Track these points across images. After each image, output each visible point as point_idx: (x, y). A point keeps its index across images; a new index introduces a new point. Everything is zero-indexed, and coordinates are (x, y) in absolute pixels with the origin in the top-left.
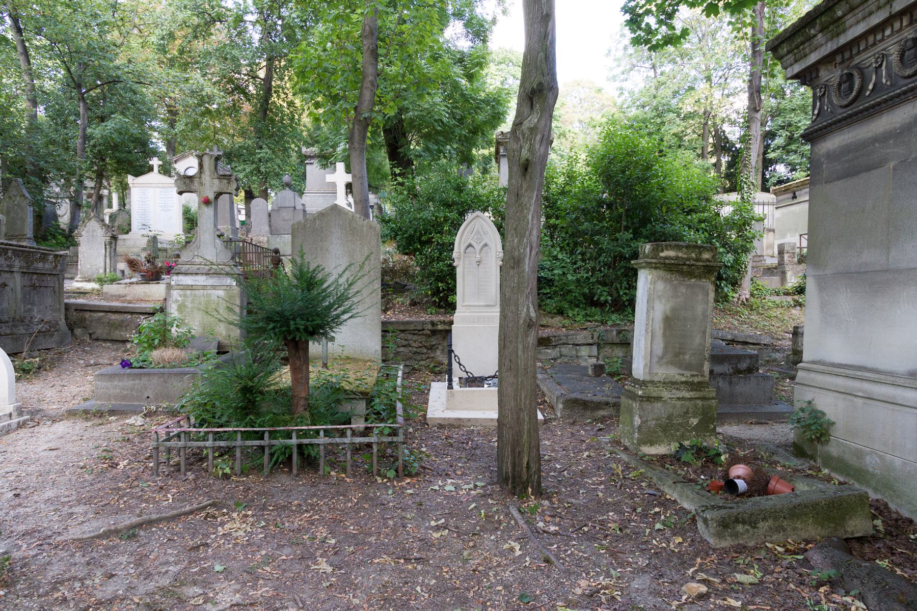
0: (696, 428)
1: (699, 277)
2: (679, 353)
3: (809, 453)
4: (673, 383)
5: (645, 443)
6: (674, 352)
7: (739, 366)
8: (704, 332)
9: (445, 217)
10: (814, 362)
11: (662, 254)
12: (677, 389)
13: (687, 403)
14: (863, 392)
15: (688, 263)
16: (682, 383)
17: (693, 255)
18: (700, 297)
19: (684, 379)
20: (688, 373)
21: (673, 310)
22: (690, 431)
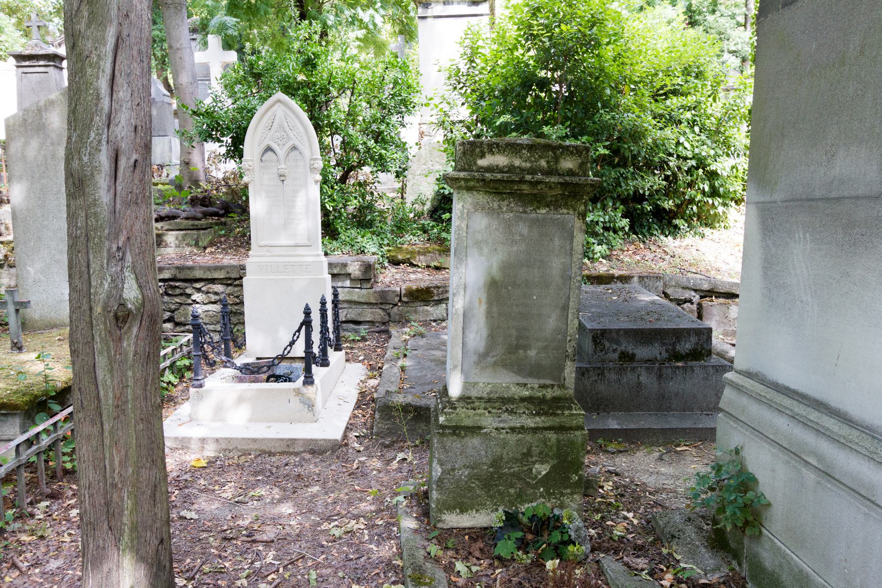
0: (545, 481)
1: (555, 204)
2: (518, 347)
3: (733, 545)
4: (504, 401)
5: (451, 508)
6: (508, 342)
7: (678, 347)
8: (565, 308)
10: (749, 375)
11: (482, 162)
12: (511, 412)
13: (529, 437)
14: (820, 458)
15: (528, 177)
16: (523, 399)
17: (543, 163)
18: (557, 242)
19: (526, 393)
20: (534, 383)
21: (506, 267)
22: (535, 487)
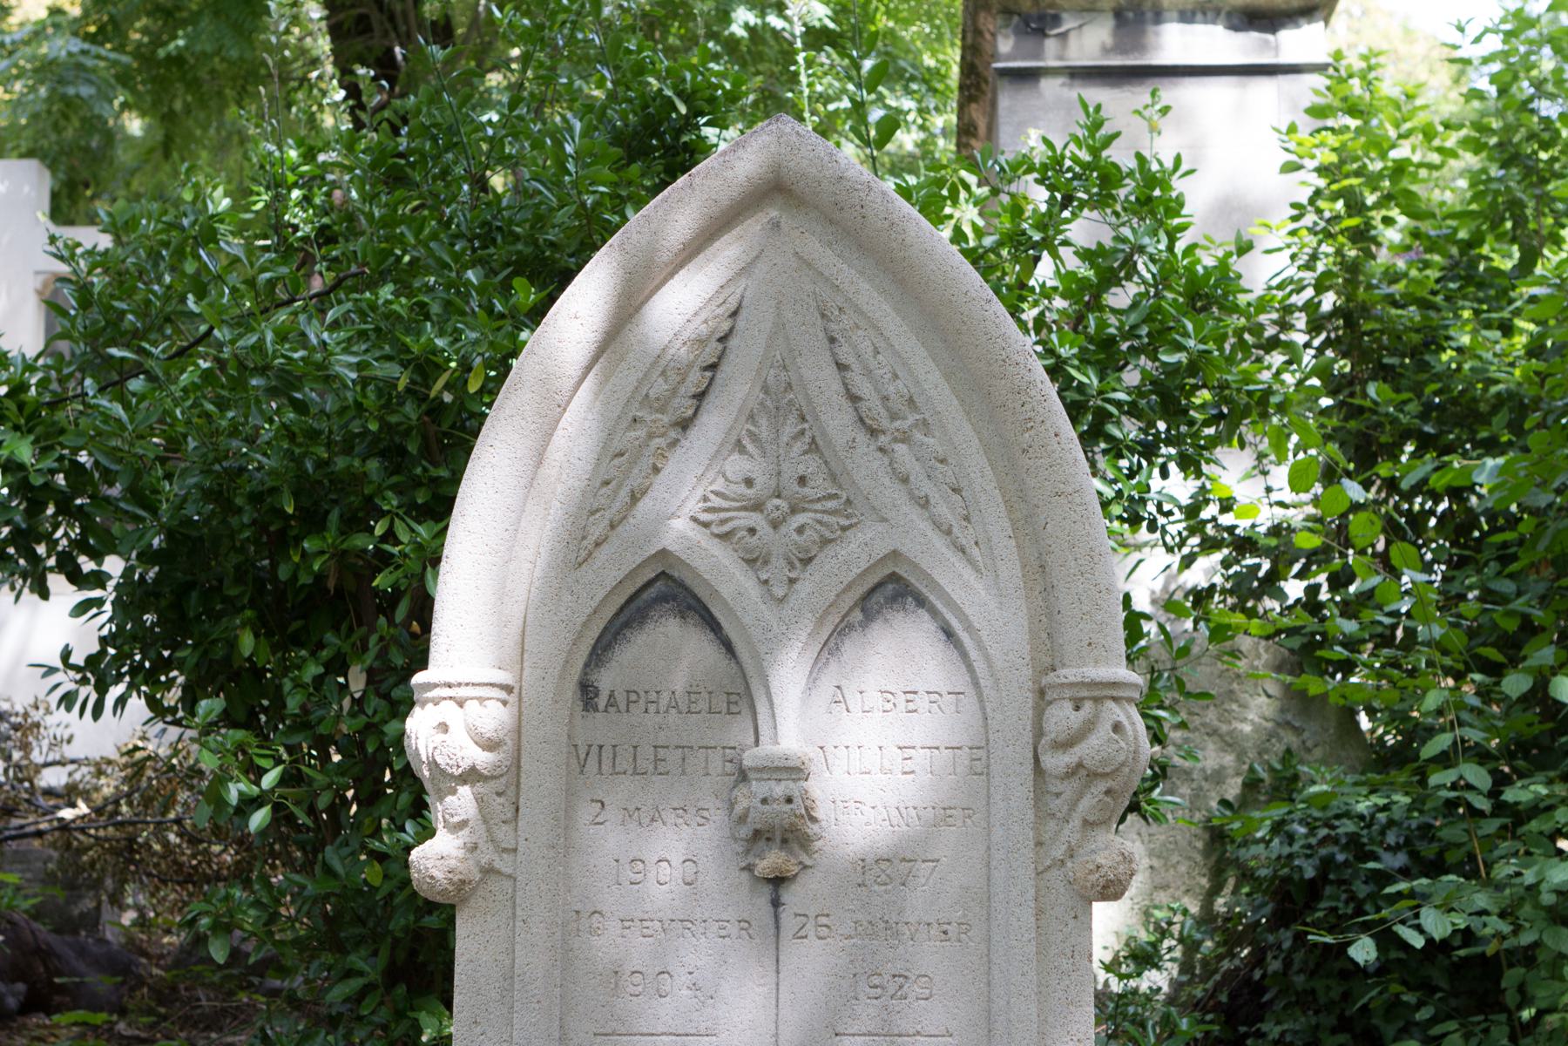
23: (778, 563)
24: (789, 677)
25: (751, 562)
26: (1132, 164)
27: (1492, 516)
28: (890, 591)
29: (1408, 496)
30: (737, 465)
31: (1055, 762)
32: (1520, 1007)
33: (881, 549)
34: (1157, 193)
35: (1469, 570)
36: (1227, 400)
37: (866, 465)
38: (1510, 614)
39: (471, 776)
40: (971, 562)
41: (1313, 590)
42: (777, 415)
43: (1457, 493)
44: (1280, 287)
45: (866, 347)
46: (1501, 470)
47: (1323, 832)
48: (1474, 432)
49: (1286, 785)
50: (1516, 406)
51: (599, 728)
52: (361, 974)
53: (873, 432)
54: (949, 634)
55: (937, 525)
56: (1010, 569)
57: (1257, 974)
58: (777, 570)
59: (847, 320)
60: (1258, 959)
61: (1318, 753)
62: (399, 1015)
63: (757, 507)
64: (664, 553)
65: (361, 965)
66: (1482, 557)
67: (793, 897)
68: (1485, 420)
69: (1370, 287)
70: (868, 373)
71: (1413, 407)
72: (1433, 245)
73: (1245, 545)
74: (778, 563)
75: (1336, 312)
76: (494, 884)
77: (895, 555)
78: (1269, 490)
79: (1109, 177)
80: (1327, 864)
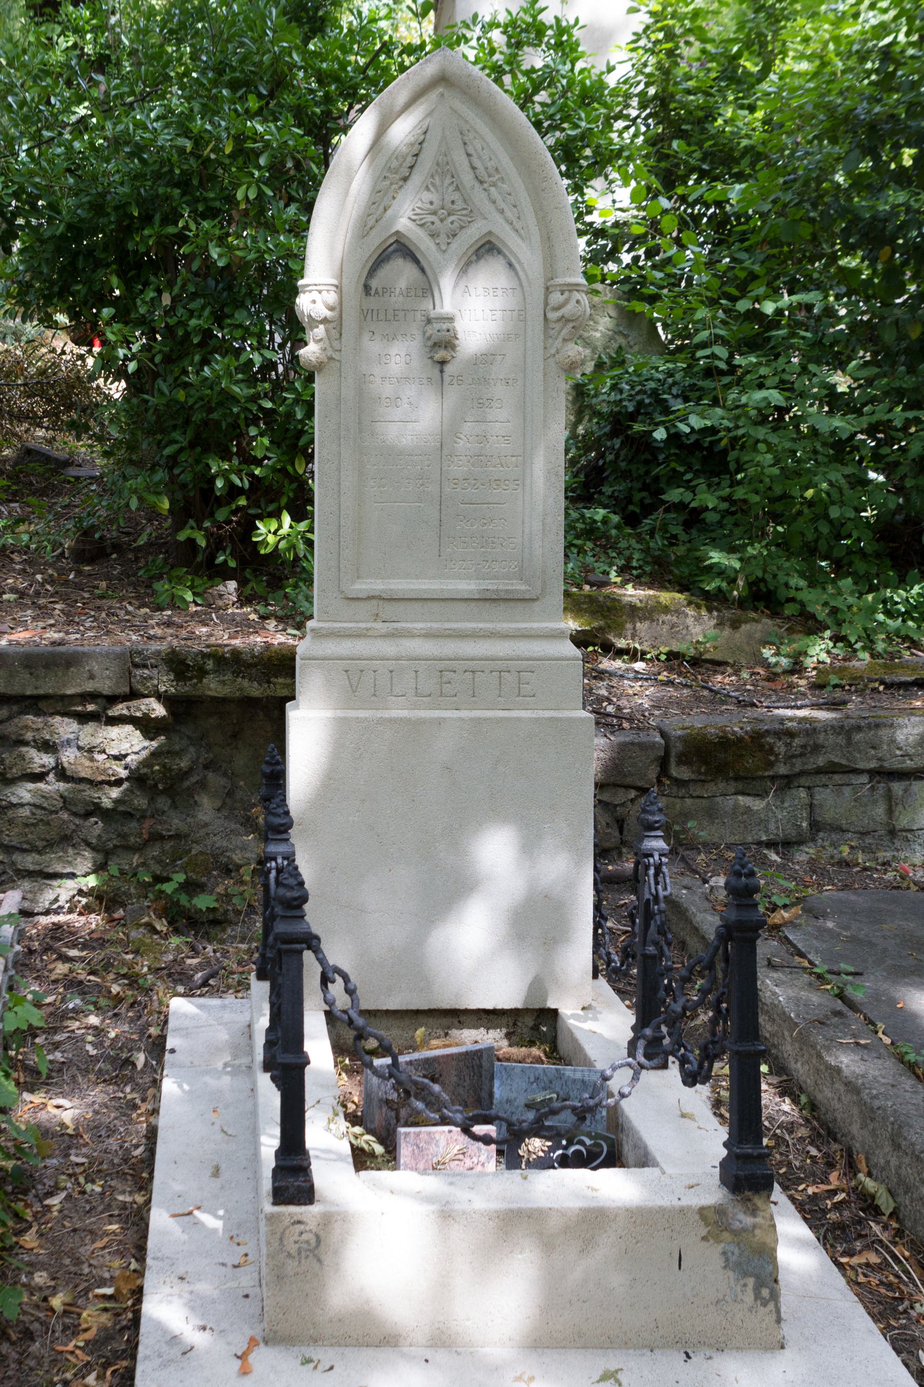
9: (239, 139)
23: (443, 236)
24: (447, 282)
25: (432, 236)
26: (553, 21)
27: (738, 217)
28: (488, 248)
29: (692, 205)
30: (427, 196)
31: (552, 316)
32: (737, 472)
33: (485, 230)
34: (565, 38)
35: (724, 247)
36: (600, 154)
37: (478, 196)
38: (743, 269)
39: (325, 321)
40: (520, 236)
41: (636, 259)
42: (443, 175)
43: (719, 204)
44: (625, 82)
45: (479, 147)
46: (743, 191)
47: (638, 388)
48: (731, 168)
49: (620, 362)
50: (755, 155)
51: (372, 302)
52: (177, 442)
53: (481, 182)
54: (511, 265)
55: (507, 221)
56: (536, 238)
57: (601, 462)
58: (443, 239)
59: (471, 135)
60: (601, 456)
61: (636, 348)
62: (198, 462)
63: (434, 213)
64: (397, 232)
65: (178, 438)
66: (731, 240)
67: (448, 368)
68: (737, 162)
69: (676, 84)
70: (480, 157)
71: (698, 155)
72: (713, 58)
73: (600, 233)
74: (443, 236)
75: (656, 96)
76: (332, 364)
77: (490, 233)
78: (614, 202)
79: (540, 29)
80: (640, 404)
